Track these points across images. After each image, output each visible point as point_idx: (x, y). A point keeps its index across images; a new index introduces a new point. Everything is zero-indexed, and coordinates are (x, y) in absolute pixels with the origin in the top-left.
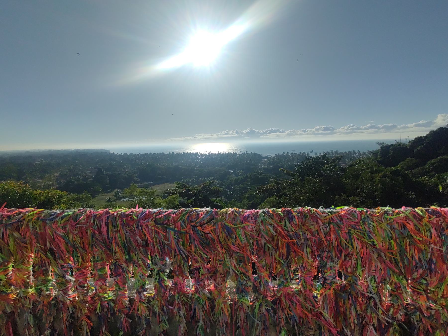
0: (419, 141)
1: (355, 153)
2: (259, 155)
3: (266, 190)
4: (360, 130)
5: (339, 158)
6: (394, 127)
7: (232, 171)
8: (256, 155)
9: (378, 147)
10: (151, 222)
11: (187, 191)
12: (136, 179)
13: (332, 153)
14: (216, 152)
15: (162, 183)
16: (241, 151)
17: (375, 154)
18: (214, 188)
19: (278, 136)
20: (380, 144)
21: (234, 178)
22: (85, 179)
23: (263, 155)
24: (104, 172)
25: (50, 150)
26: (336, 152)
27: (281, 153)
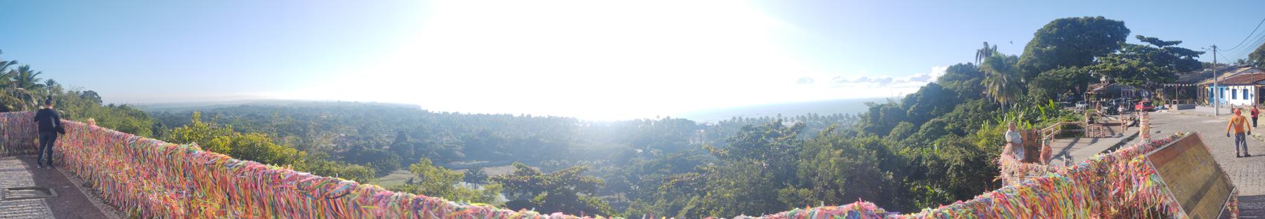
0: (911, 99)
1: (841, 117)
2: (692, 123)
3: (679, 184)
4: (1227, 75)
5: (285, 109)
6: (889, 80)
8: (685, 121)
9: (866, 110)
10: (294, 184)
11: (533, 181)
12: (458, 153)
15: (503, 165)
17: (864, 118)
18: (587, 178)
20: (868, 104)
21: (643, 161)
22: (378, 146)
23: (698, 121)
24: (409, 139)
25: (668, 121)
26: (816, 116)
27: (729, 119)
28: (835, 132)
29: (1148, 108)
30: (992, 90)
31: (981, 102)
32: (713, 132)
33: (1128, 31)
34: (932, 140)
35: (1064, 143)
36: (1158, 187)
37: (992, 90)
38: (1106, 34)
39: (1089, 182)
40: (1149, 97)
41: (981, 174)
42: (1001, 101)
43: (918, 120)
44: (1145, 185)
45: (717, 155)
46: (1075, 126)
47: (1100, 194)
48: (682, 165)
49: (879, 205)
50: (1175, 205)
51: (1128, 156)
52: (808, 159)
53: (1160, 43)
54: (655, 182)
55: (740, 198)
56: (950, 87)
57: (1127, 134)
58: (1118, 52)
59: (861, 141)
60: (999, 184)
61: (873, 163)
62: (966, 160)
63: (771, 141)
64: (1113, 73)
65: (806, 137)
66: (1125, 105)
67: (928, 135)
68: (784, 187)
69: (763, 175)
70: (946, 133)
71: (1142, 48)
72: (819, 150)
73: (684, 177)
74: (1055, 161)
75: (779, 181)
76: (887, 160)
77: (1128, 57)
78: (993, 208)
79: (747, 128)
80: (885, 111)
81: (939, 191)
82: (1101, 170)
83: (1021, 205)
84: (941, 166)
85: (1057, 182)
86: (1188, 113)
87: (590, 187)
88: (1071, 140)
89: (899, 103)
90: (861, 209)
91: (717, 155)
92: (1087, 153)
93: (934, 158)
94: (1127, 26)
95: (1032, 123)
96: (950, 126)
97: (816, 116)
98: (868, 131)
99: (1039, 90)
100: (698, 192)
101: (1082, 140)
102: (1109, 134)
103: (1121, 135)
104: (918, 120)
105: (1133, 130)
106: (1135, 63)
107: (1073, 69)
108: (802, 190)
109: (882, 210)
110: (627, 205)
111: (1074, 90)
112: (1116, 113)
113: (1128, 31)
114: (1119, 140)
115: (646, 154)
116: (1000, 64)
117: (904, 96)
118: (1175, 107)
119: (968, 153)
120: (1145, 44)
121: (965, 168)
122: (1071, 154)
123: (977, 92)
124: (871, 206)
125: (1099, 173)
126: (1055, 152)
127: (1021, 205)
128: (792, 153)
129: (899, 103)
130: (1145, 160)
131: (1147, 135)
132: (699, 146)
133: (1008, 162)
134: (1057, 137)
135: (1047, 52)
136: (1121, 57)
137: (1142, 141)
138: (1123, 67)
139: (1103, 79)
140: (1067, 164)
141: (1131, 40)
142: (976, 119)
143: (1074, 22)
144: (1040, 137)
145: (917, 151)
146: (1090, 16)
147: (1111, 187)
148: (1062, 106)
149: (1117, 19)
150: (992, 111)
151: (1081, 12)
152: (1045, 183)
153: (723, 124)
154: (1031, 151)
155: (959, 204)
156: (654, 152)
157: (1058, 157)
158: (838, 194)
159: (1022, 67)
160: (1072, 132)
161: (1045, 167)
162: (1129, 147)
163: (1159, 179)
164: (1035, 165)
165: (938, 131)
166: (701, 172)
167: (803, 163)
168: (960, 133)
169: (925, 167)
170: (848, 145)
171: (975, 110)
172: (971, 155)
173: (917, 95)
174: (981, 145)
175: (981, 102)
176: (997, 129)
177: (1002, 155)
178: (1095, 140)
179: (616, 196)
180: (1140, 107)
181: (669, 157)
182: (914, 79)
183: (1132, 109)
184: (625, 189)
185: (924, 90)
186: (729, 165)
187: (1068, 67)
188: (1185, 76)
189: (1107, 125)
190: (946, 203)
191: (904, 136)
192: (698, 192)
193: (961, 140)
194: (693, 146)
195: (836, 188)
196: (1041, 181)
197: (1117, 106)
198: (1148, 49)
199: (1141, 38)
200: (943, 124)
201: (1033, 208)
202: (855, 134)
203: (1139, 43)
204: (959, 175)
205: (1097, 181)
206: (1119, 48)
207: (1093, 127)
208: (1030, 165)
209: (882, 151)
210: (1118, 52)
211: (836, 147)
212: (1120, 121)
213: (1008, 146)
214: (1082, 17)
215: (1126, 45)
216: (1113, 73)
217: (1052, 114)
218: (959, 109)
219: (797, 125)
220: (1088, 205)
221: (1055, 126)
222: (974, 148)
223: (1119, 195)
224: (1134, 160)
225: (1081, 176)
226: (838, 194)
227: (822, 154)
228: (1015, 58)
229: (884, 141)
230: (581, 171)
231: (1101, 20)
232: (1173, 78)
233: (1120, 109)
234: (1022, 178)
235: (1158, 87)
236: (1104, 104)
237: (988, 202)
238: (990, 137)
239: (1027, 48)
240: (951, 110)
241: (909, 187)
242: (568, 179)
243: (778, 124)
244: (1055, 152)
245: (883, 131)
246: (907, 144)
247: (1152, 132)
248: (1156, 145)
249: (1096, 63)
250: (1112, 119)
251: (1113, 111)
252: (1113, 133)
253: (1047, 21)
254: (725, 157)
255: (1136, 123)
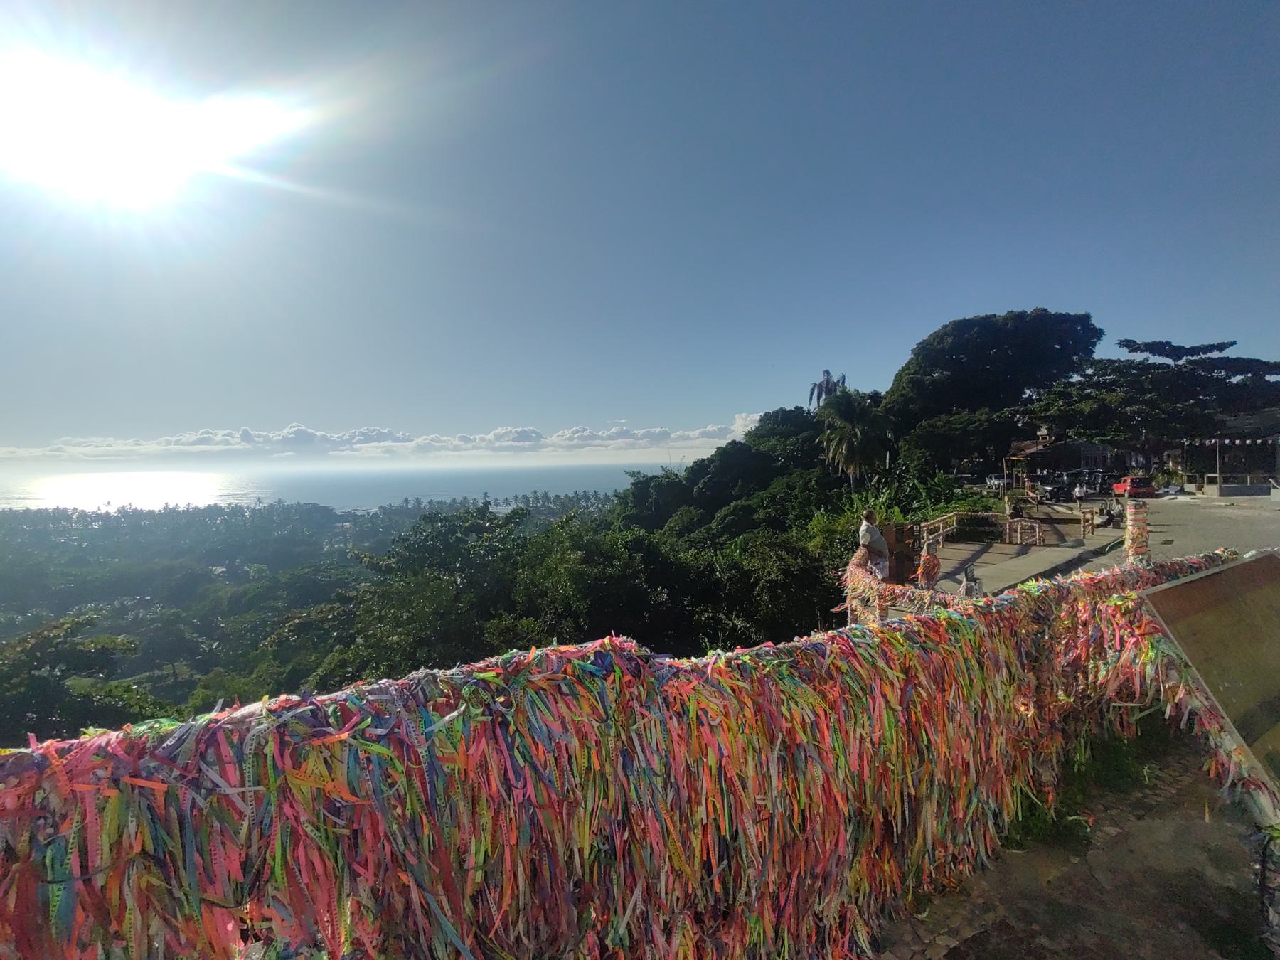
0: (700, 468)
3: (302, 629)
6: (665, 435)
7: (220, 569)
8: (315, 508)
9: (626, 484)
13: (536, 498)
14: (157, 507)
16: (259, 500)
17: (622, 498)
19: (388, 451)
20: (632, 474)
21: (227, 590)
26: (546, 495)
27: (397, 502)
28: (576, 522)
29: (1142, 490)
30: (835, 452)
31: (815, 473)
32: (365, 525)
33: (1099, 334)
34: (733, 536)
35: (961, 551)
36: (1170, 665)
37: (835, 452)
38: (1051, 342)
39: (1015, 634)
40: (1146, 467)
41: (816, 602)
42: (850, 471)
43: (711, 502)
44: (1143, 658)
45: (375, 567)
46: (985, 521)
47: (1036, 659)
48: (308, 592)
49: (642, 642)
50: (1212, 711)
51: (1099, 589)
52: (532, 568)
53: (1176, 352)
54: (254, 629)
55: (422, 642)
56: (764, 447)
57: (1092, 542)
58: (1076, 378)
59: (621, 537)
60: (842, 620)
61: (636, 574)
62: (786, 572)
63: (472, 539)
64: (1062, 422)
65: (530, 531)
66: (1090, 484)
67: (726, 529)
68: (493, 617)
69: (457, 598)
70: (756, 525)
71: (1130, 364)
72: (550, 552)
73: (313, 613)
74: (945, 584)
75: (484, 609)
76: (661, 568)
77: (1097, 386)
78: (828, 661)
79: (430, 518)
80: (659, 487)
81: (739, 623)
82: (1041, 613)
83: (881, 663)
84: (744, 579)
85: (953, 626)
86: (1247, 508)
87: (102, 662)
88: (976, 547)
89: (682, 474)
90: (614, 647)
91: (375, 567)
92: (1012, 574)
93: (735, 566)
94: (1096, 322)
95: (905, 512)
96: (761, 514)
97: (546, 496)
98: (629, 521)
99: (918, 453)
100: (339, 640)
101: (997, 547)
102: (1052, 539)
103: (1080, 543)
104: (711, 502)
105: (1109, 535)
106: (1113, 398)
107: (982, 415)
108: (524, 621)
109: (646, 651)
110: (192, 685)
111: (983, 454)
112: (1070, 499)
113: (1099, 334)
114: (1075, 552)
115: (234, 574)
116: (844, 404)
117: (689, 462)
118: (1211, 490)
119: (790, 561)
120: (1138, 357)
121: (784, 586)
122: (978, 573)
123: (809, 456)
124: (629, 644)
125: (1037, 619)
126: (946, 567)
127: (881, 663)
128: (505, 559)
129: (682, 474)
130: (1140, 603)
131: (1141, 547)
132: (343, 553)
133: (859, 580)
134: (950, 539)
135: (933, 382)
136: (1081, 386)
137: (1130, 560)
138: (1087, 407)
139: (1043, 432)
140: (969, 592)
141: (1105, 350)
142: (807, 502)
143: (987, 325)
144: (918, 538)
145: (707, 554)
146: (1017, 309)
147: (1060, 648)
148: (959, 482)
149: (1073, 308)
150: (832, 491)
151: (959, 318)
152: (931, 625)
153: (386, 511)
154: (900, 563)
155: (767, 647)
156: (251, 569)
157: (951, 576)
158: (578, 628)
159: (888, 411)
160: (979, 531)
161: (927, 595)
162: (1103, 570)
163: (1173, 649)
164: (909, 589)
165: (742, 523)
166: (346, 600)
167: (524, 574)
168: (779, 525)
169: (719, 581)
170: (597, 543)
171: (805, 487)
172: (796, 564)
173: (711, 460)
174: (813, 546)
175: (815, 473)
176: (842, 520)
177: (850, 568)
178: (1024, 549)
179: (167, 670)
180: (1125, 486)
181: (284, 578)
182: (703, 435)
183: (1106, 492)
184: (185, 649)
185: (721, 452)
186: (397, 583)
187: (972, 411)
188: (1247, 421)
189: (1049, 520)
190: (748, 643)
191: (687, 529)
192: (339, 640)
193: (780, 538)
194: (330, 554)
195: (575, 615)
196: (923, 623)
197: (1072, 486)
198: (1144, 367)
199: (1130, 345)
200: (750, 510)
201: (906, 670)
202: (608, 525)
203: (1124, 355)
204: (774, 598)
205: (1031, 635)
206: (1079, 369)
207: (1020, 524)
208: (898, 589)
209: (651, 553)
210: (1076, 378)
211: (576, 546)
212: (1077, 513)
213: (861, 552)
214: (1001, 312)
215: (1094, 363)
216: (1062, 422)
217: (941, 497)
218: (778, 486)
219: (514, 513)
220: (1012, 679)
221: (946, 518)
222: (802, 552)
223: (1077, 666)
224: (1115, 600)
225: (999, 619)
226: (578, 628)
227: (552, 560)
228: (875, 397)
229: (656, 537)
230: (76, 629)
231: (1042, 316)
232: (1211, 427)
233: (1077, 492)
234: (884, 614)
235: (1168, 446)
236: (1044, 481)
237: (819, 650)
238: (829, 533)
239: (898, 378)
240: (764, 485)
241: (692, 614)
242: (44, 652)
243: (483, 511)
244: (946, 567)
245: (653, 523)
246: (692, 543)
247: (1154, 540)
248: (1165, 572)
249: (1030, 400)
250: (1061, 510)
251: (1062, 494)
252: (1062, 538)
253: (935, 327)
254: (389, 570)
255: (1114, 521)
